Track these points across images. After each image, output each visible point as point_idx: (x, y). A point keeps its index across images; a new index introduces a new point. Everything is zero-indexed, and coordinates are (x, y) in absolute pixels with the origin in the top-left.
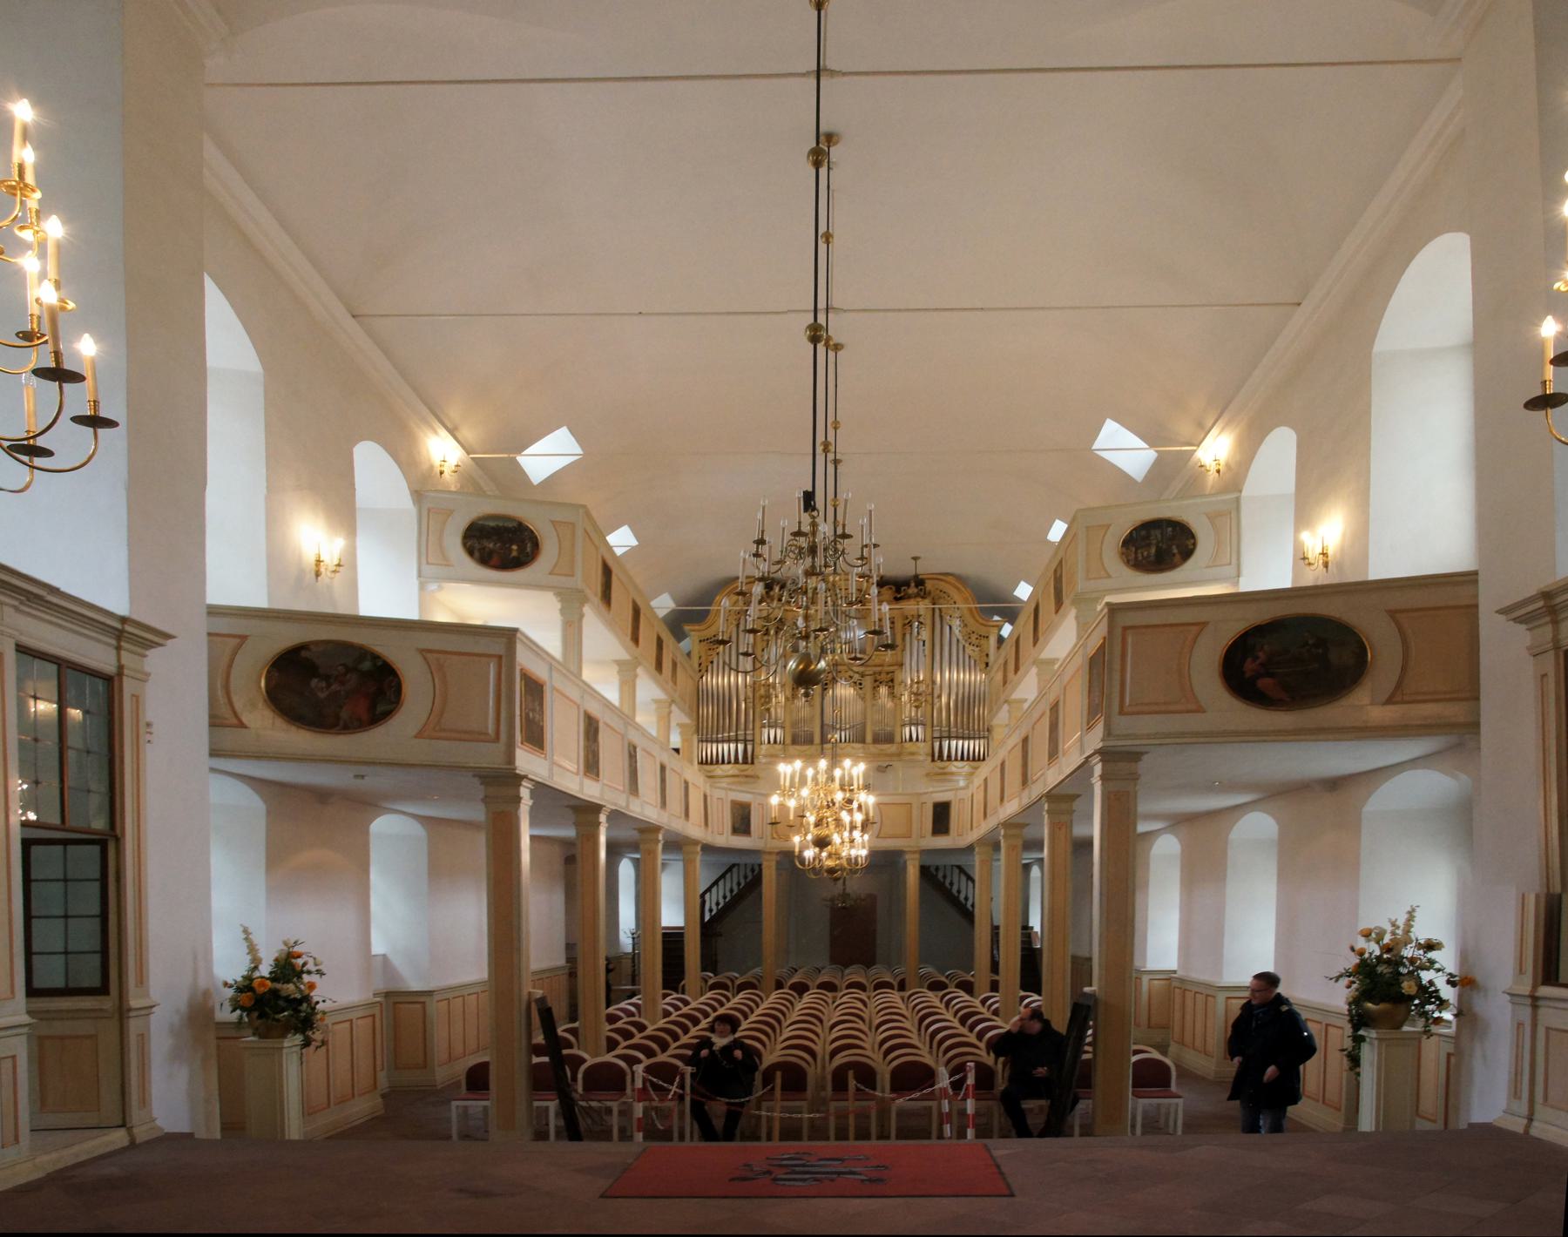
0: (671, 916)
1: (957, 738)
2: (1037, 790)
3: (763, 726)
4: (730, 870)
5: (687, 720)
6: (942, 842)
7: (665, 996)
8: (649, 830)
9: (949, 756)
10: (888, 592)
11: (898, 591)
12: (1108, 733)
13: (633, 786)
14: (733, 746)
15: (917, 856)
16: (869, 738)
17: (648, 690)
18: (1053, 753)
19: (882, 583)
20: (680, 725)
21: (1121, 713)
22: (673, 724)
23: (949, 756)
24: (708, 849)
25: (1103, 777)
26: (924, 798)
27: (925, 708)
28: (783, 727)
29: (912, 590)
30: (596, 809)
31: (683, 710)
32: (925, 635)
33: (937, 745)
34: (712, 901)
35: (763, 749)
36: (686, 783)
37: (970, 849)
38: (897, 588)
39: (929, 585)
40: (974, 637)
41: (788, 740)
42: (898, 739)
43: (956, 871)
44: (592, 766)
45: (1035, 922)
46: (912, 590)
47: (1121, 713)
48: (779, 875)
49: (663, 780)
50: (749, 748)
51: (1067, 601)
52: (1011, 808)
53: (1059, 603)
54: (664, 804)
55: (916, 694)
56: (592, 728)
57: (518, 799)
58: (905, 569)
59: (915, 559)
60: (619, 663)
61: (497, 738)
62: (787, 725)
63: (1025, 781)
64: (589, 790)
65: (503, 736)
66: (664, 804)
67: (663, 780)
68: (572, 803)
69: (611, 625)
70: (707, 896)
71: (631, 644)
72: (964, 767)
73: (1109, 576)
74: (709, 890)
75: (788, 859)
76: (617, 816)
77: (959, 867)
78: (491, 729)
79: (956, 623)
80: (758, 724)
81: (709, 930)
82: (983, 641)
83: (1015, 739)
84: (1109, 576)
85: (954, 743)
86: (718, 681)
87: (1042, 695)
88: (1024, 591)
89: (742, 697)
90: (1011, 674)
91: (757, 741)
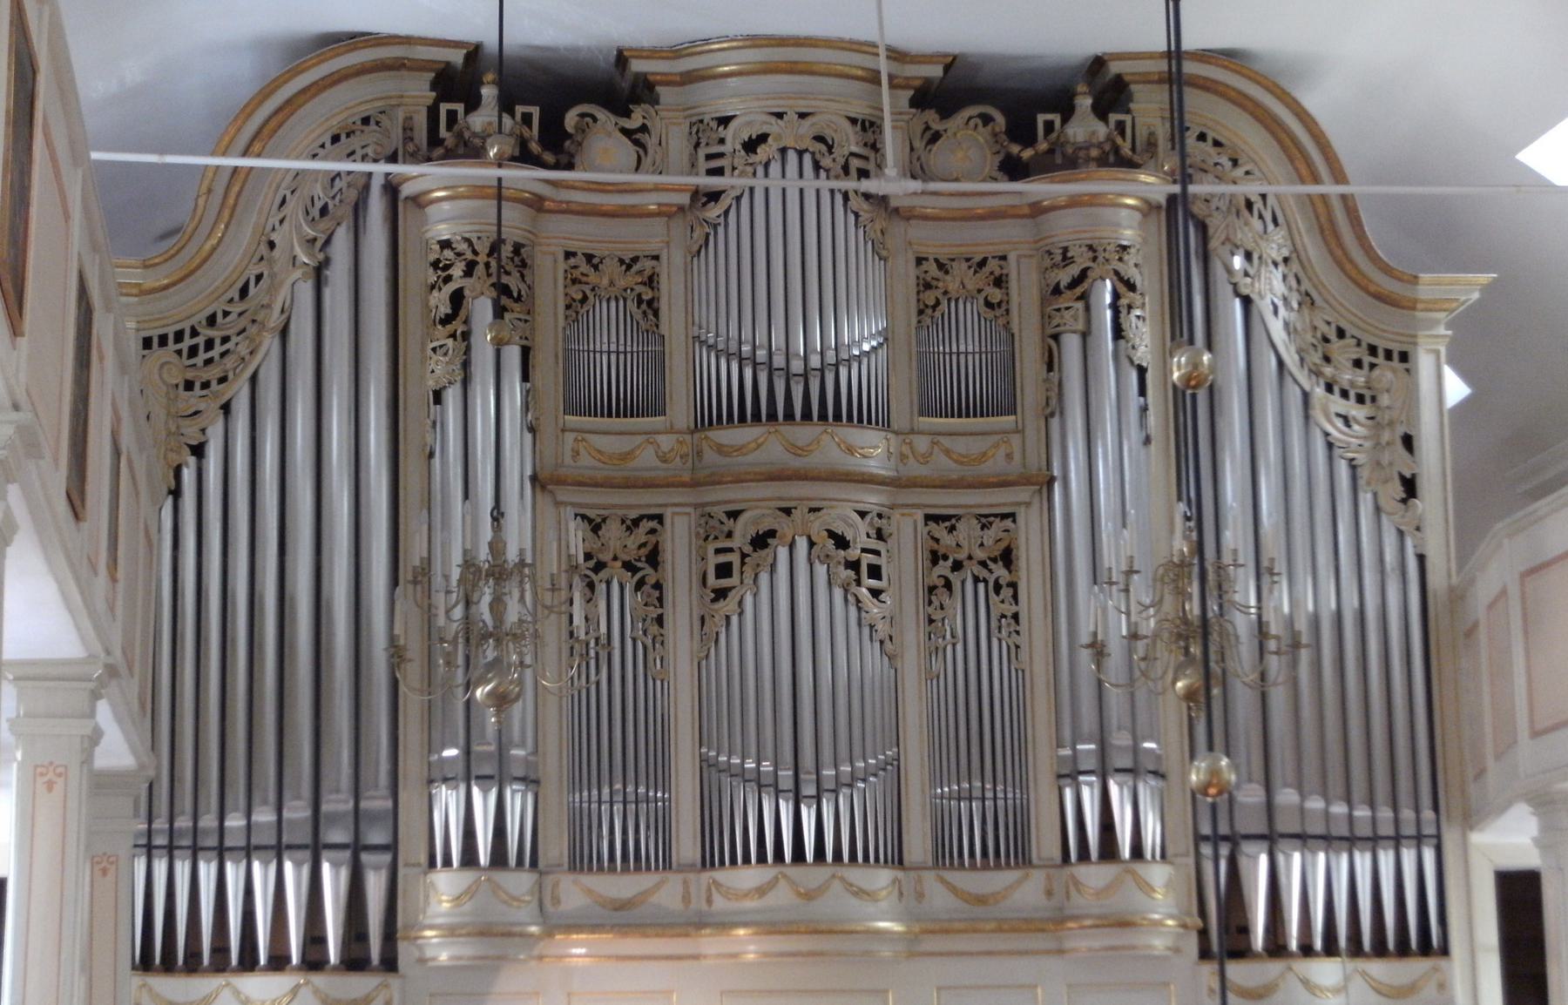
3: (437, 776)
10: (969, 142)
11: (1021, 131)
14: (1363, 862)
16: (918, 844)
17: (459, 570)
28: (531, 781)
29: (1085, 128)
35: (442, 894)
40: (1343, 352)
41: (556, 848)
42: (1045, 844)
46: (1085, 128)
50: (375, 887)
62: (554, 767)
79: (1272, 287)
80: (411, 765)
82: (1387, 374)
85: (1386, 860)
90: (79, 509)
91: (413, 849)
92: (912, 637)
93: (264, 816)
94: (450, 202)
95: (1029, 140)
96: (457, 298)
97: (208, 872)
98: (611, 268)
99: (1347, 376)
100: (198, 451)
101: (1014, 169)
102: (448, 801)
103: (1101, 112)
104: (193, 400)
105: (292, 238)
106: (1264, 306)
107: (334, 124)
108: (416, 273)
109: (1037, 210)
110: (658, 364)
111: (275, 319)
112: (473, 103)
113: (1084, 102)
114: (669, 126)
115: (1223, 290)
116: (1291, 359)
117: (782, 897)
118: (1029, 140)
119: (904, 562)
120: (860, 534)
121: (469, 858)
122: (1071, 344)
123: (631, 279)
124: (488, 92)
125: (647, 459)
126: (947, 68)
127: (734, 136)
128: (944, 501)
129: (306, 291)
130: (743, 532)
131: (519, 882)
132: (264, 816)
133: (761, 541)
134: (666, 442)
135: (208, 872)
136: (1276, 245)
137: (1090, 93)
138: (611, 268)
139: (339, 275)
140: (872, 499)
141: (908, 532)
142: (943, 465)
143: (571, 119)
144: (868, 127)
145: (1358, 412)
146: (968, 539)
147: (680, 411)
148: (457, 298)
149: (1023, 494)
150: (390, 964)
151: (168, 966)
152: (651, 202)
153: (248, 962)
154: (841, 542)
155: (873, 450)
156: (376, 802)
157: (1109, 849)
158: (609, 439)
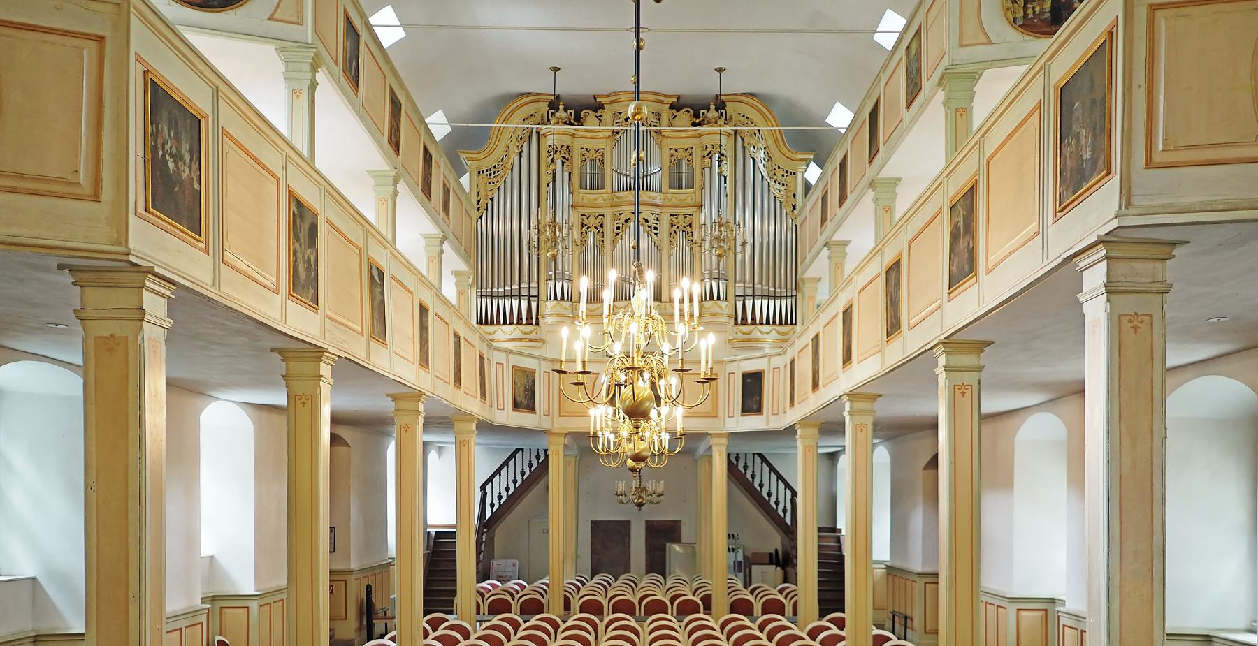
0: (441, 511)
1: (762, 296)
2: (911, 342)
4: (513, 456)
5: (462, 266)
6: (753, 423)
7: (435, 624)
8: (407, 396)
9: (753, 319)
10: (684, 116)
11: (697, 115)
12: (1126, 200)
13: (378, 327)
14: (765, 302)
15: (724, 441)
18: (963, 267)
19: (676, 106)
20: (457, 274)
21: (1149, 165)
22: (447, 273)
23: (753, 319)
24: (486, 428)
25: (1111, 289)
26: (730, 368)
27: (727, 260)
29: (712, 114)
30: (317, 353)
31: (457, 251)
32: (727, 170)
33: (739, 304)
34: (494, 491)
36: (456, 336)
37: (790, 431)
38: (698, 109)
39: (730, 108)
43: (758, 460)
44: (304, 284)
45: (842, 523)
47: (1149, 165)
48: (567, 463)
49: (424, 328)
50: (534, 305)
51: (926, 86)
52: (864, 370)
53: (914, 89)
54: (425, 360)
55: (719, 239)
56: (304, 225)
57: (319, 378)
58: (707, 86)
59: (720, 70)
60: (375, 175)
61: (96, 197)
63: (893, 326)
64: (298, 321)
65: (107, 193)
66: (425, 360)
67: (424, 328)
68: (279, 343)
69: (363, 112)
70: (488, 488)
71: (391, 151)
72: (772, 332)
73: (990, 42)
74: (490, 480)
75: (583, 443)
76: (350, 370)
77: (761, 455)
78: (84, 177)
79: (760, 155)
81: (486, 526)
82: (790, 178)
83: (877, 267)
84: (990, 42)
85: (758, 302)
86: (498, 227)
87: (948, 171)
88: (840, 117)
89: (525, 241)
91: (542, 297)
92: (665, 244)
93: (508, 288)
94: (556, 133)
95: (698, 117)
96: (553, 160)
97: (495, 302)
98: (592, 152)
99: (780, 179)
100: (492, 199)
101: (694, 124)
102: (551, 284)
103: (717, 109)
104: (489, 187)
105: (513, 146)
106: (758, 161)
107: (523, 116)
108: (544, 154)
109: (700, 135)
110: (603, 177)
111: (509, 166)
112: (557, 110)
113: (713, 107)
114: (607, 113)
115: (748, 156)
116: (765, 175)
117: (774, 335)
118: (698, 117)
119: (664, 227)
120: (652, 219)
121: (555, 298)
122: (707, 170)
123: (598, 154)
124: (561, 107)
125: (600, 200)
126: (678, 99)
127: (623, 117)
128: (674, 211)
129: (517, 158)
130: (623, 218)
131: (566, 304)
132: (508, 288)
133: (626, 221)
134: (605, 196)
135: (495, 302)
136: (762, 145)
137: (84, 370)
138: (592, 152)
139: (525, 154)
140: (656, 210)
141: (665, 219)
142: (674, 201)
143: (582, 114)
144: (657, 115)
145: (783, 188)
146: (681, 221)
147: (609, 187)
148: (553, 160)
149: (694, 209)
150: (537, 324)
151: (486, 323)
152: (601, 135)
153: (505, 323)
154: (647, 221)
155: (656, 197)
156: (534, 285)
157: (712, 298)
158: (591, 196)
